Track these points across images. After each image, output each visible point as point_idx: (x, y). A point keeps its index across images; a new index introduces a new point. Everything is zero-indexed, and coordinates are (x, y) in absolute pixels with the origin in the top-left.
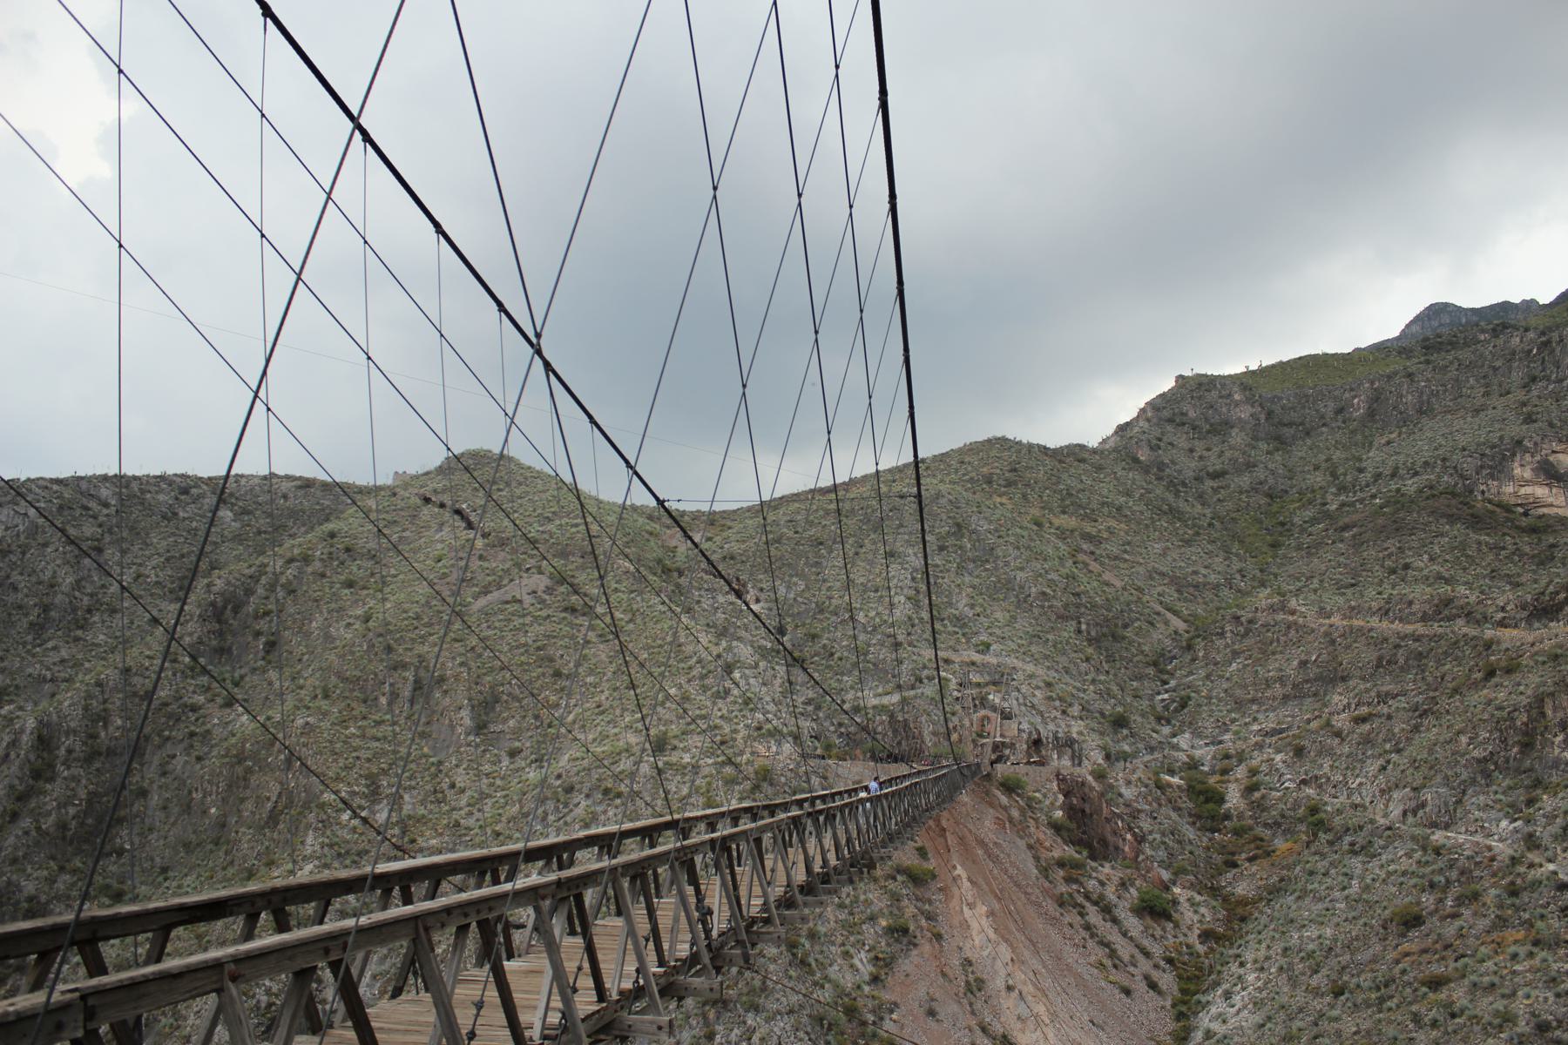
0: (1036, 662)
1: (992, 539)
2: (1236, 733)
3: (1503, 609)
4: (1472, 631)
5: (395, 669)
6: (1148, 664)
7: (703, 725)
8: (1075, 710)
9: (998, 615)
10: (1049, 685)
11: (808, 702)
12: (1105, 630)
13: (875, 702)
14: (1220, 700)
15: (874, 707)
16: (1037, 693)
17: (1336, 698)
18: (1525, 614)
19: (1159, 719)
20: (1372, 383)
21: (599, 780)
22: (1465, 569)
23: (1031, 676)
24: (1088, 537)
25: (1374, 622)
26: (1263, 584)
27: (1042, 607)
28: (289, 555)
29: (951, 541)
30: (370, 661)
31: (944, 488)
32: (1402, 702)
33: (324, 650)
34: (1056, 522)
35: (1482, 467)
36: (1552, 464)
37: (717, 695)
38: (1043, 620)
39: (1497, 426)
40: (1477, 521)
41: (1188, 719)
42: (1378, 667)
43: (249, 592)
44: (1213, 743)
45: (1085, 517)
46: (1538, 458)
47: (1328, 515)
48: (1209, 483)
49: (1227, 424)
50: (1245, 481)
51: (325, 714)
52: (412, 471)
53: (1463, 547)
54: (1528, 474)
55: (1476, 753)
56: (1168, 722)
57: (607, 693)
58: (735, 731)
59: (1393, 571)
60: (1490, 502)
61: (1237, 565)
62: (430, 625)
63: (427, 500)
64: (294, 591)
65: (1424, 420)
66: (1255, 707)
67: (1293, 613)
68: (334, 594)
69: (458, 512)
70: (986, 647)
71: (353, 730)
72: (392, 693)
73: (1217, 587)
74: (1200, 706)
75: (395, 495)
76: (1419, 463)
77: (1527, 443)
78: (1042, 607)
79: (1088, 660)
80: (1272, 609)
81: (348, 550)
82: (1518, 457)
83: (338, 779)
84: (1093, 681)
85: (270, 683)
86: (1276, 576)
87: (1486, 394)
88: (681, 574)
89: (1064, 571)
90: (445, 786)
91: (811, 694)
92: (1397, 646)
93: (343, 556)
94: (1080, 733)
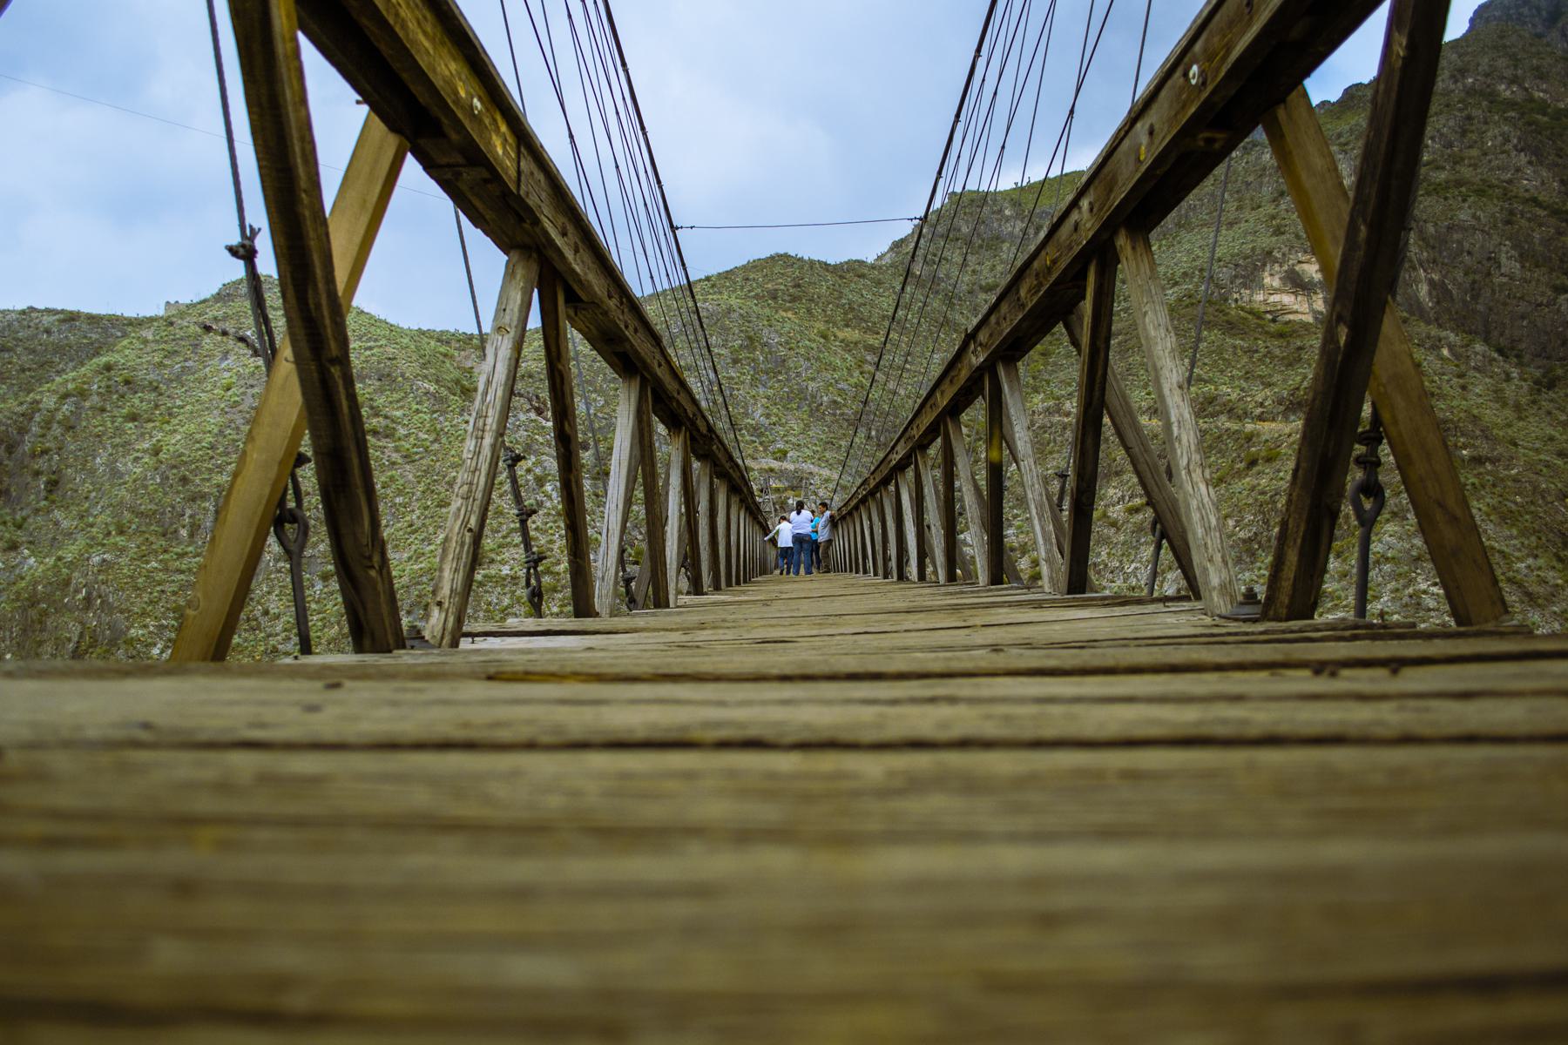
0: (831, 467)
3: (1262, 405)
4: (1234, 426)
5: (194, 500)
9: (793, 423)
17: (1111, 491)
18: (1282, 408)
21: (419, 596)
22: (1222, 372)
26: (1036, 390)
28: (62, 390)
29: (743, 355)
30: (166, 494)
31: (733, 302)
33: (112, 486)
34: (841, 335)
38: (835, 427)
39: (1250, 238)
40: (1231, 327)
43: (22, 431)
45: (867, 330)
46: (1286, 268)
49: (999, 239)
51: (123, 550)
52: (185, 300)
53: (1220, 351)
54: (1276, 283)
55: (1242, 535)
57: (418, 512)
60: (1242, 309)
62: (227, 454)
63: (208, 329)
64: (72, 428)
65: (1183, 233)
68: (117, 429)
69: (242, 339)
71: (154, 564)
72: (192, 525)
75: (172, 324)
76: (1178, 274)
80: (1048, 411)
81: (127, 382)
83: (144, 614)
85: (57, 523)
86: (1048, 382)
87: (1239, 208)
89: (853, 381)
90: (258, 613)
93: (123, 389)
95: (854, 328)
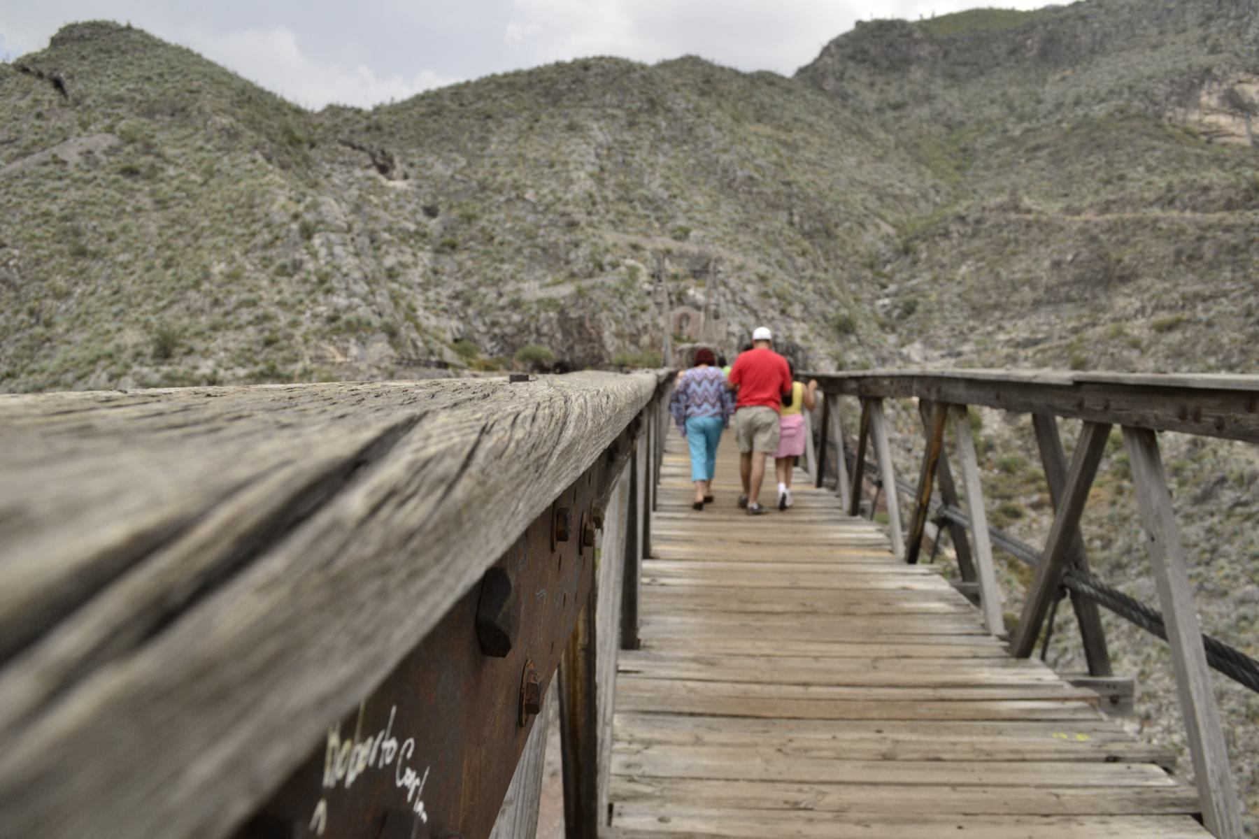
1: (690, 119)
2: (978, 343)
6: (865, 265)
7: (246, 315)
8: (796, 310)
9: (699, 199)
10: (763, 279)
11: (456, 296)
12: (818, 225)
13: (541, 294)
14: (954, 305)
15: (539, 301)
16: (750, 288)
19: (883, 326)
20: (1045, 25)
23: (741, 268)
24: (784, 143)
25: (1156, 212)
27: (750, 193)
29: (643, 118)
32: (1225, 305)
35: (1171, 93)
36: (1237, 94)
37: (283, 271)
41: (916, 327)
42: (1176, 263)
44: (950, 355)
45: (778, 128)
46: (1225, 87)
47: (1012, 140)
48: (890, 114)
50: (925, 111)
54: (1214, 102)
56: (893, 330)
58: (295, 324)
59: (1109, 182)
61: (929, 182)
65: (1098, 58)
66: (997, 314)
67: (1029, 211)
70: (683, 234)
73: (914, 200)
74: (930, 312)
77: (1215, 71)
78: (750, 193)
79: (804, 254)
80: (1003, 208)
82: (1206, 86)
84: (812, 279)
87: (1161, 33)
88: (312, 146)
91: (460, 286)
92: (1200, 239)
94: (804, 338)
95: (766, 124)
